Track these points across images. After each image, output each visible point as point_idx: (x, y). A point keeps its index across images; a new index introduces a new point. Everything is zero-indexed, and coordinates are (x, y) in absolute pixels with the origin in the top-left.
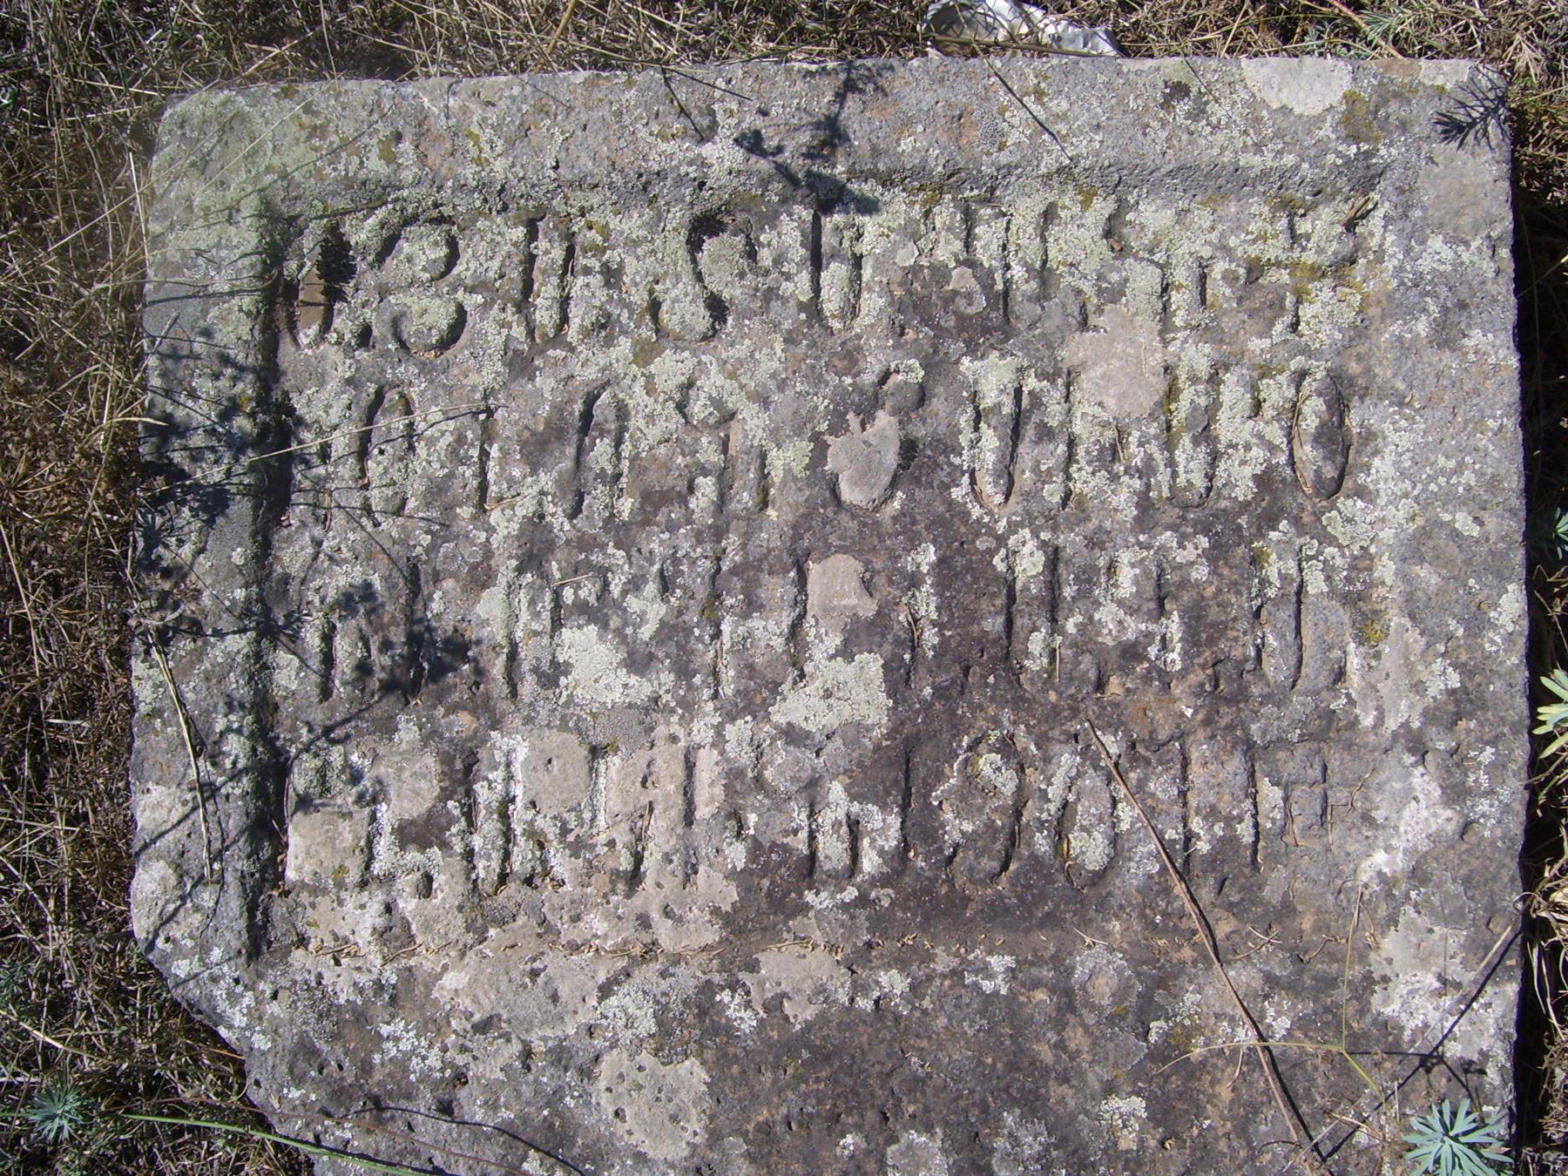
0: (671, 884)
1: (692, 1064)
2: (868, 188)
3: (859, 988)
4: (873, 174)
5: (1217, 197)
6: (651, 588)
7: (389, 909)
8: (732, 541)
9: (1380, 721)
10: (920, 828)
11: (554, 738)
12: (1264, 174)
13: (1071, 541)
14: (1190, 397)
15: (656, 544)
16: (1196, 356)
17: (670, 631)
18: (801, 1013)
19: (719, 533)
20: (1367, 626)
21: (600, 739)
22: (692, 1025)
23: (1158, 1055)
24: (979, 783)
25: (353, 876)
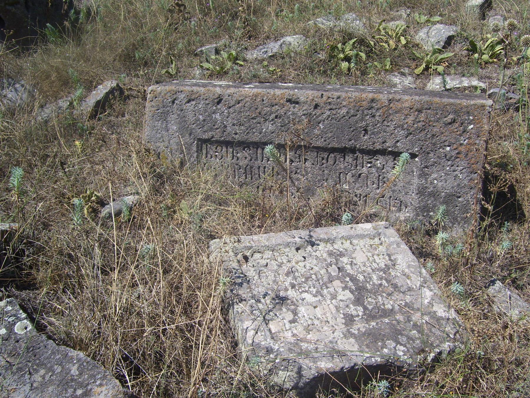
0: (334, 321)
1: (351, 339)
2: (318, 242)
3: (369, 325)
4: (318, 240)
5: (362, 239)
6: (312, 288)
7: (292, 332)
8: (320, 281)
9: (416, 286)
10: (365, 308)
11: (308, 307)
12: (367, 235)
13: (366, 274)
14: (371, 259)
15: (310, 283)
16: (370, 254)
17: (317, 292)
18: (363, 330)
19: (318, 280)
20: (408, 277)
21: (315, 305)
22: (348, 334)
23: (413, 325)
24: (370, 301)
25: (284, 329)
